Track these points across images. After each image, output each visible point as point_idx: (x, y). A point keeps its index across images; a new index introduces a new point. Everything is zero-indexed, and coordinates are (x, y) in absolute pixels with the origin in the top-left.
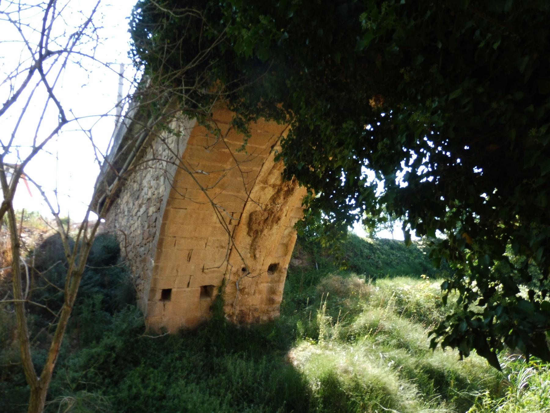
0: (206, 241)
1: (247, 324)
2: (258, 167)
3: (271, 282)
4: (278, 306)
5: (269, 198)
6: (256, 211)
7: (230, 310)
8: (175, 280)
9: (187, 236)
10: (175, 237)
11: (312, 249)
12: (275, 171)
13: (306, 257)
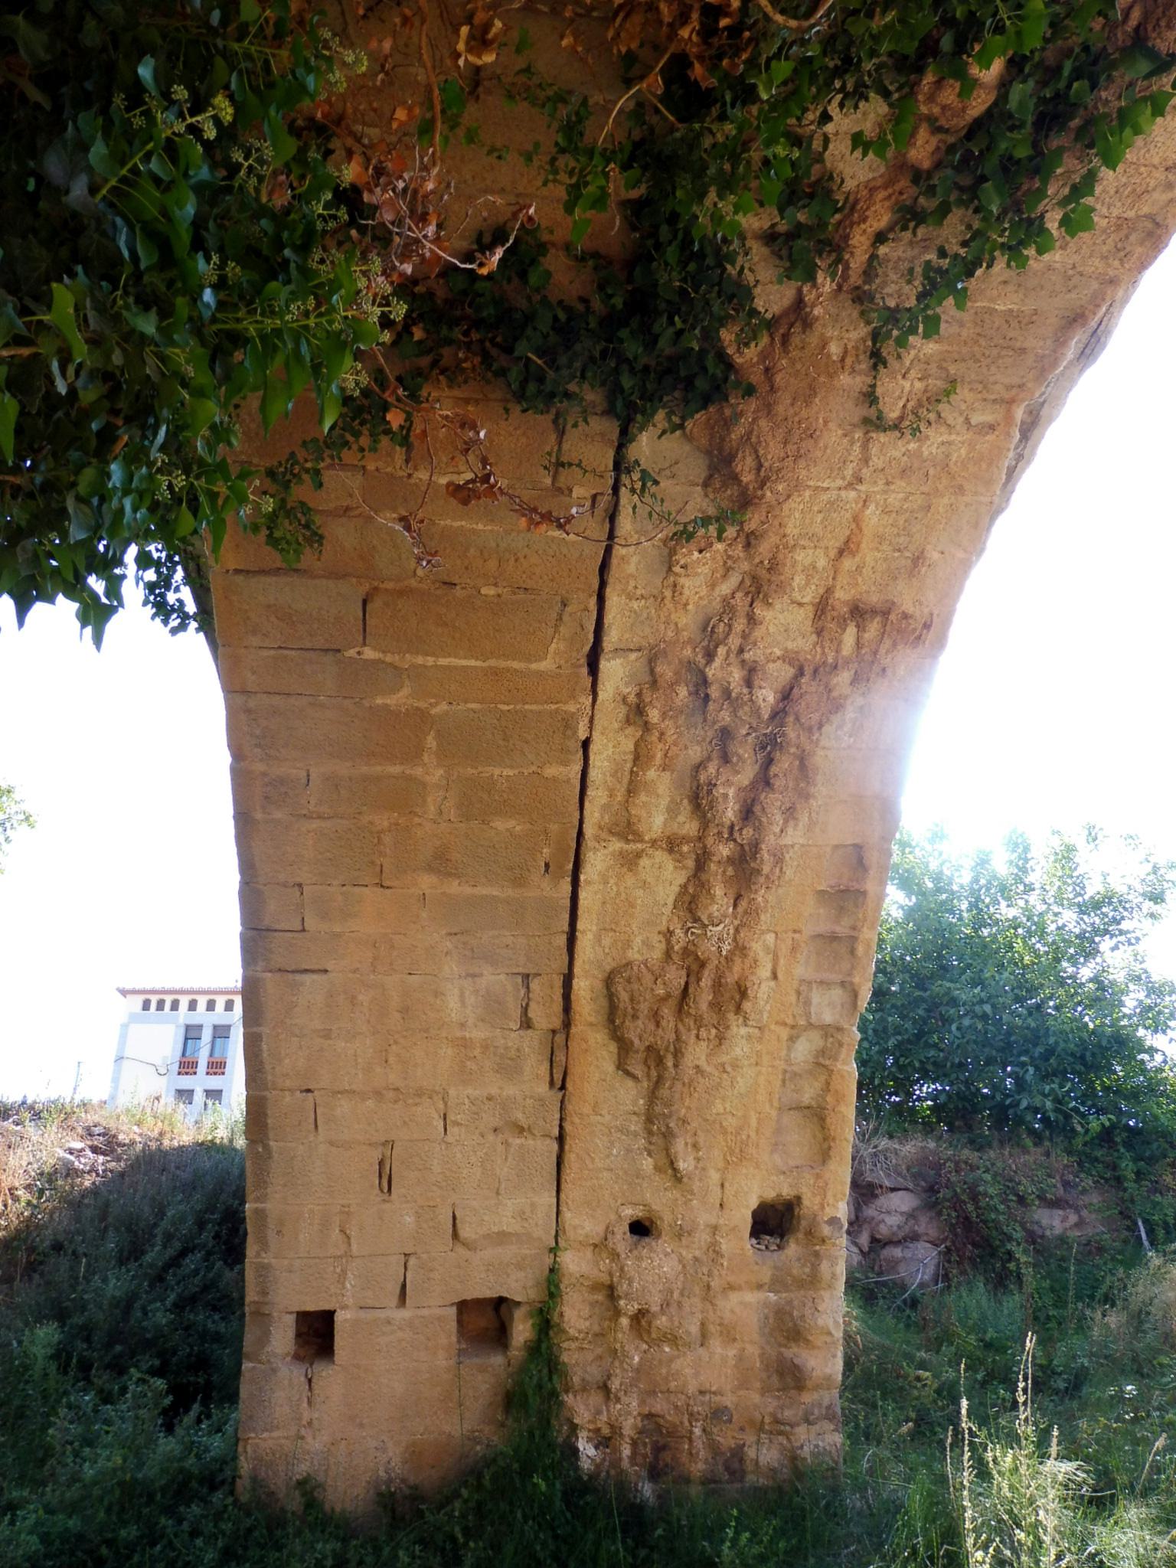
0: (441, 1105)
1: (688, 1481)
2: (565, 763)
3: (777, 1284)
4: (831, 1397)
5: (670, 901)
6: (629, 964)
7: (599, 1412)
8: (344, 1272)
9: (354, 1087)
10: (308, 1091)
11: (1115, 1167)
12: (652, 774)
13: (1095, 1199)
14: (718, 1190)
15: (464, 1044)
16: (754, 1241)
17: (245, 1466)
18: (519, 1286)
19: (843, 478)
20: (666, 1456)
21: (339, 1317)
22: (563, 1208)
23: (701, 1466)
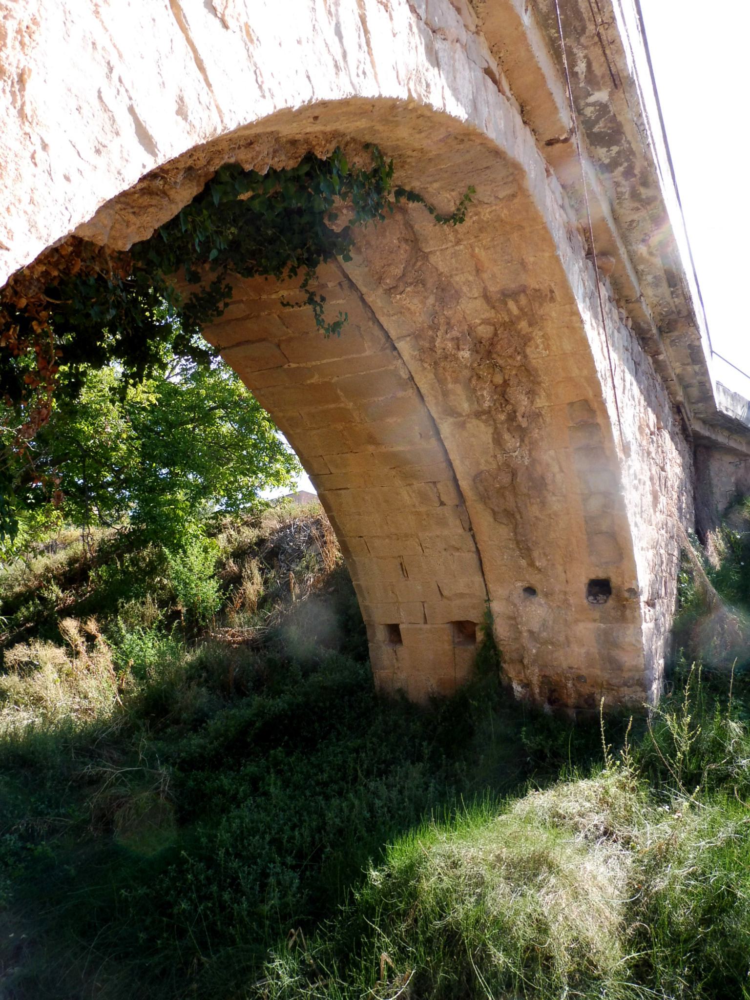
1: (567, 706)
7: (520, 673)
14: (563, 574)
15: (418, 514)
16: (591, 598)
17: (377, 683)
18: (474, 616)
19: (451, 241)
20: (556, 695)
21: (401, 627)
22: (488, 583)
23: (573, 700)
